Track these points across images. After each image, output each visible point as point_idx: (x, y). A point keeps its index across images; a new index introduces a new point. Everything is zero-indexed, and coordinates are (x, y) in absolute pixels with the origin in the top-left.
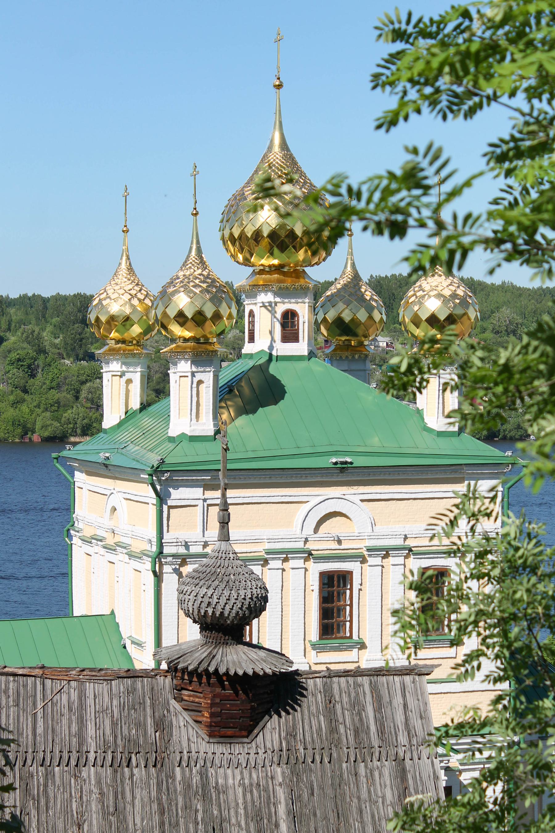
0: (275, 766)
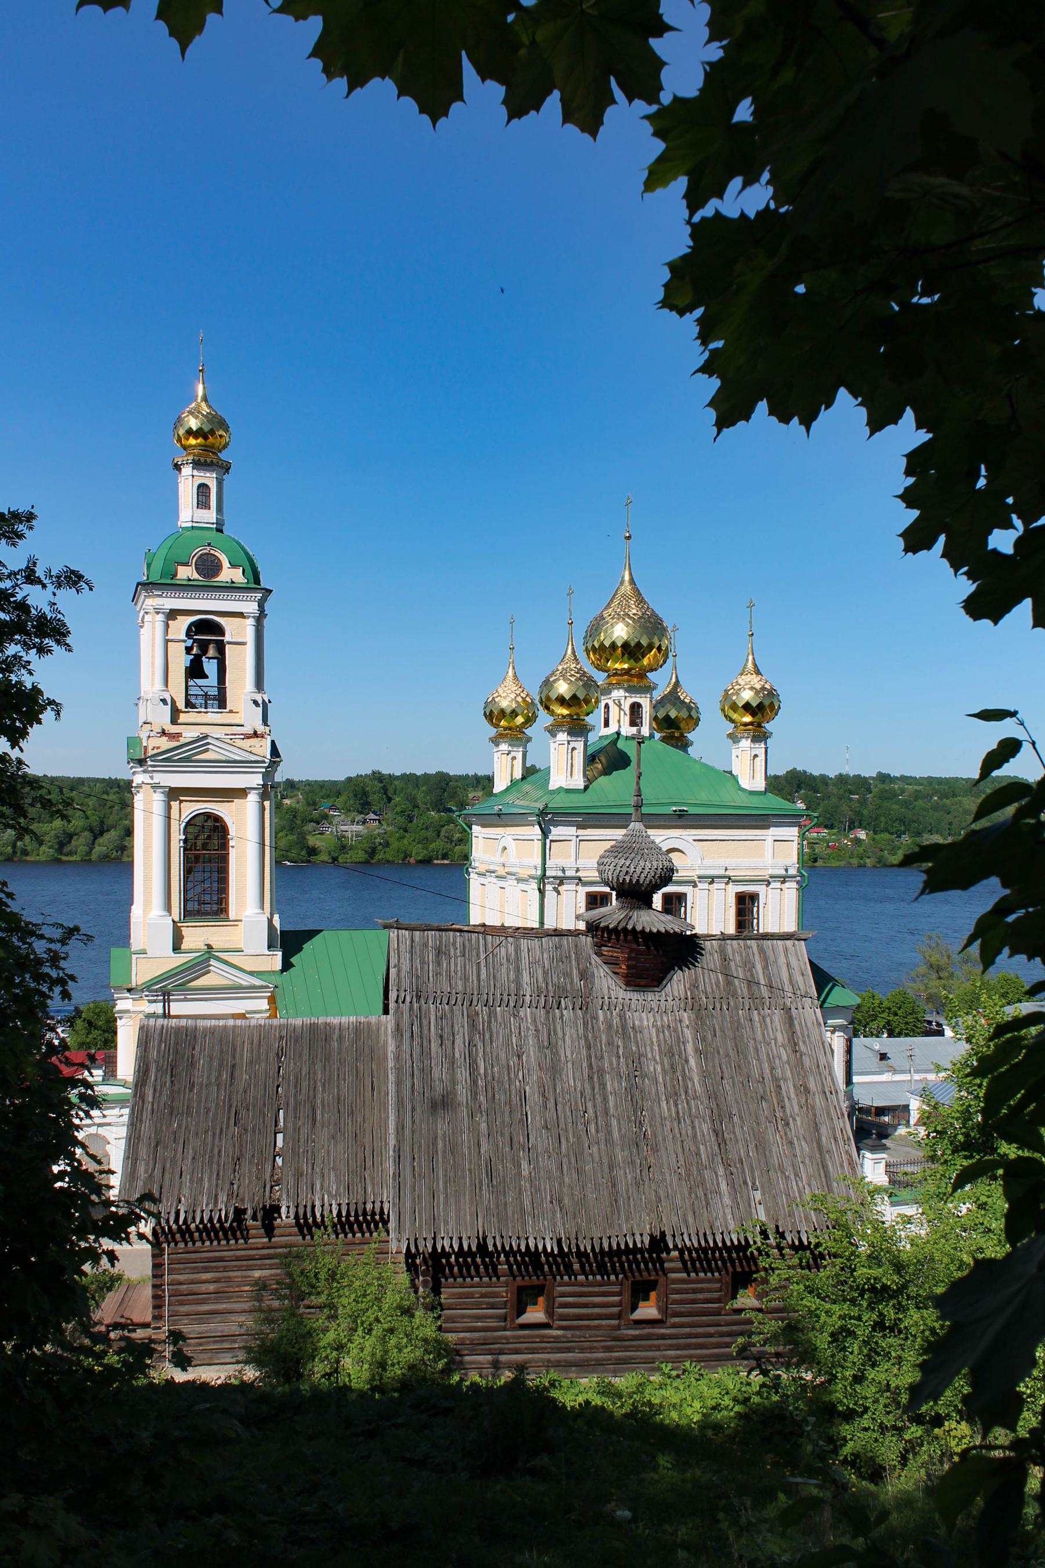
0: (682, 1011)
